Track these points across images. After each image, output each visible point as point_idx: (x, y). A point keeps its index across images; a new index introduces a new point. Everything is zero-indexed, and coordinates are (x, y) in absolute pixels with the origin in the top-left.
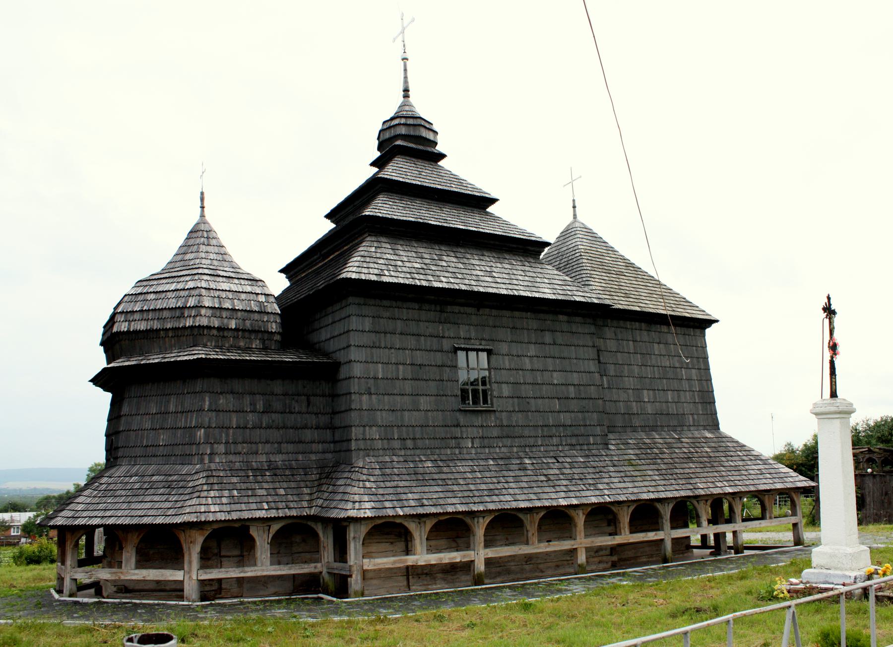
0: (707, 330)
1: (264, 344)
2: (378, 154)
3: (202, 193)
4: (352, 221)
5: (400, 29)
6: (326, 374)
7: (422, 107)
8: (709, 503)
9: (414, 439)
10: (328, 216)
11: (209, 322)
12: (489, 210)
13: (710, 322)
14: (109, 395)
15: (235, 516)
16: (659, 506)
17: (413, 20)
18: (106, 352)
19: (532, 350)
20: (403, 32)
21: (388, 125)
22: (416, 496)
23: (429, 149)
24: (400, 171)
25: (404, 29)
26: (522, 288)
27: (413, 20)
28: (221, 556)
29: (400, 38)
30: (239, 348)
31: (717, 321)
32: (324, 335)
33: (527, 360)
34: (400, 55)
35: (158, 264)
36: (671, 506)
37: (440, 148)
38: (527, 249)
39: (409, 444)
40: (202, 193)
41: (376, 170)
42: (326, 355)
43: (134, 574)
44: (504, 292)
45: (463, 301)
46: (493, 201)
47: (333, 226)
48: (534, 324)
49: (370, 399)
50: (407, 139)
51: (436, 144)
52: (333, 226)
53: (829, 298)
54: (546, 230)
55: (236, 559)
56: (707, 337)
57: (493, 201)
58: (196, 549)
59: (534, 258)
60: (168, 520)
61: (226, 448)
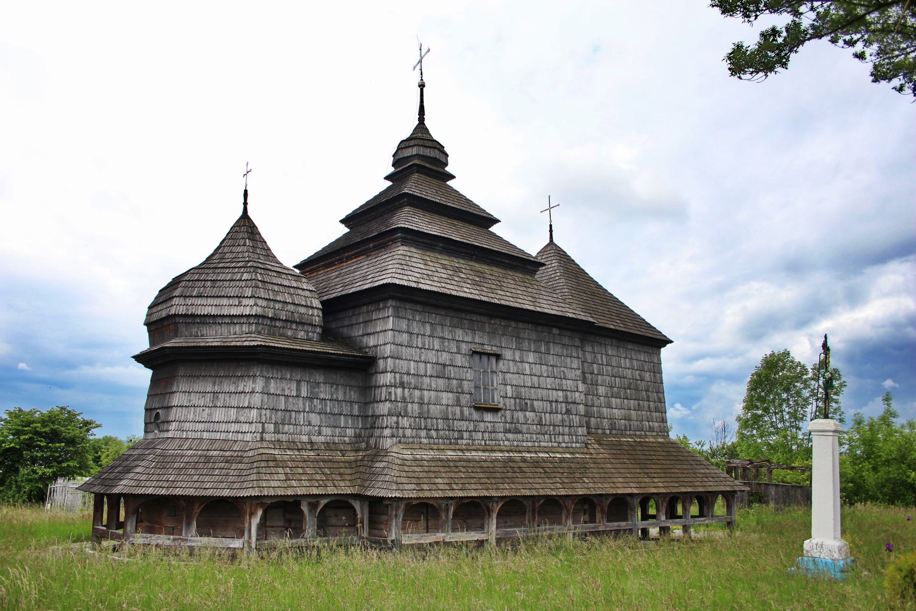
0: (662, 349)
1: (308, 335)
2: (392, 169)
3: (246, 191)
4: (369, 228)
5: (418, 58)
6: (359, 368)
7: (436, 134)
8: (667, 499)
9: (437, 430)
10: (342, 221)
11: (264, 311)
12: (492, 229)
13: (665, 342)
14: (149, 373)
15: (290, 492)
16: (629, 499)
17: (429, 50)
18: (149, 331)
19: (531, 357)
20: (420, 62)
21: (404, 145)
22: (446, 481)
23: (440, 170)
24: (412, 187)
25: (422, 58)
26: (527, 302)
27: (429, 50)
28: (266, 526)
29: (418, 67)
30: (288, 337)
31: (671, 342)
32: (357, 332)
33: (527, 366)
34: (417, 80)
35: (195, 252)
36: (639, 500)
37: (448, 169)
38: (520, 264)
39: (434, 433)
40: (246, 191)
41: (389, 183)
42: (361, 349)
43: (194, 541)
44: (571, 315)
45: (399, 295)
46: (497, 221)
47: (347, 230)
48: (534, 336)
49: (403, 392)
50: (421, 159)
51: (447, 165)
52: (347, 230)
53: (826, 337)
54: (531, 245)
55: (279, 530)
56: (662, 356)
57: (497, 221)
58: (256, 521)
59: (531, 276)
60: (233, 493)
61: (275, 428)
